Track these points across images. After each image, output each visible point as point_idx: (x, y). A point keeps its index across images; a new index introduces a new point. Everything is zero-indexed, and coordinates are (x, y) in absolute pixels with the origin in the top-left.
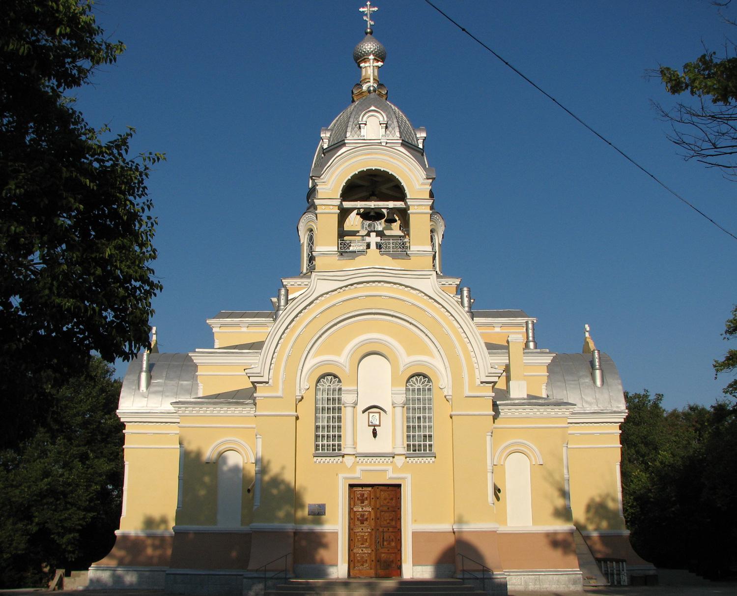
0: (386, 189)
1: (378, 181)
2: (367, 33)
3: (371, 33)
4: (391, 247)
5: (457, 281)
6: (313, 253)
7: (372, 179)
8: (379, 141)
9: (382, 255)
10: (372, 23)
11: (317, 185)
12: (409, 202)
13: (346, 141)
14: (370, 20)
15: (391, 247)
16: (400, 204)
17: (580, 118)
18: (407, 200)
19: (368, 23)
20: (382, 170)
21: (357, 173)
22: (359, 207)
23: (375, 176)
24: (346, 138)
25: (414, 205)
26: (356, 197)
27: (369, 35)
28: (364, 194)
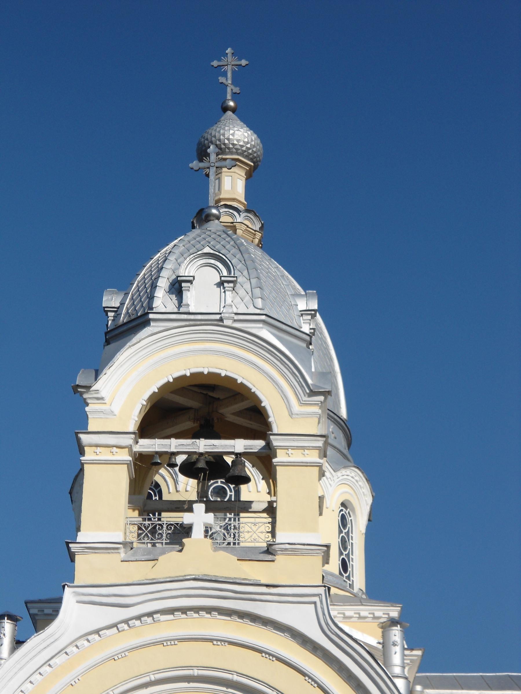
0: (234, 414)
1: (218, 399)
2: (225, 109)
3: (234, 111)
4: (164, 535)
5: (393, 611)
6: (71, 545)
7: (206, 394)
8: (218, 317)
9: (216, 550)
10: (237, 90)
11: (87, 405)
12: (276, 441)
13: (151, 316)
14: (233, 83)
15: (164, 535)
16: (258, 444)
17: (245, 305)
18: (272, 437)
19: (229, 90)
20: (223, 375)
21: (239, 382)
22: (173, 449)
23: (212, 388)
24: (152, 309)
25: (286, 448)
26: (169, 431)
27: (229, 113)
28: (188, 425)
